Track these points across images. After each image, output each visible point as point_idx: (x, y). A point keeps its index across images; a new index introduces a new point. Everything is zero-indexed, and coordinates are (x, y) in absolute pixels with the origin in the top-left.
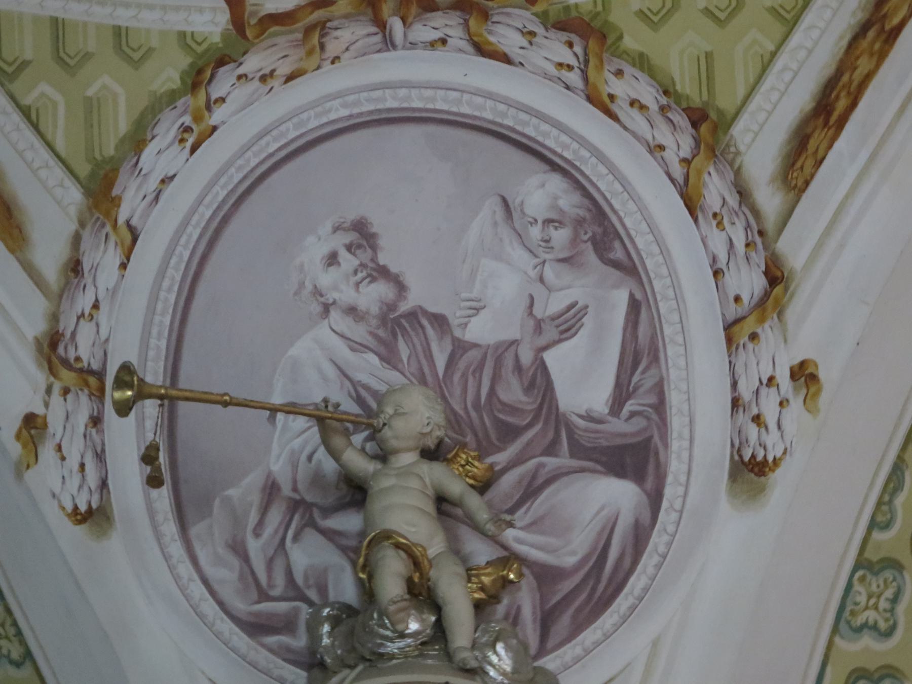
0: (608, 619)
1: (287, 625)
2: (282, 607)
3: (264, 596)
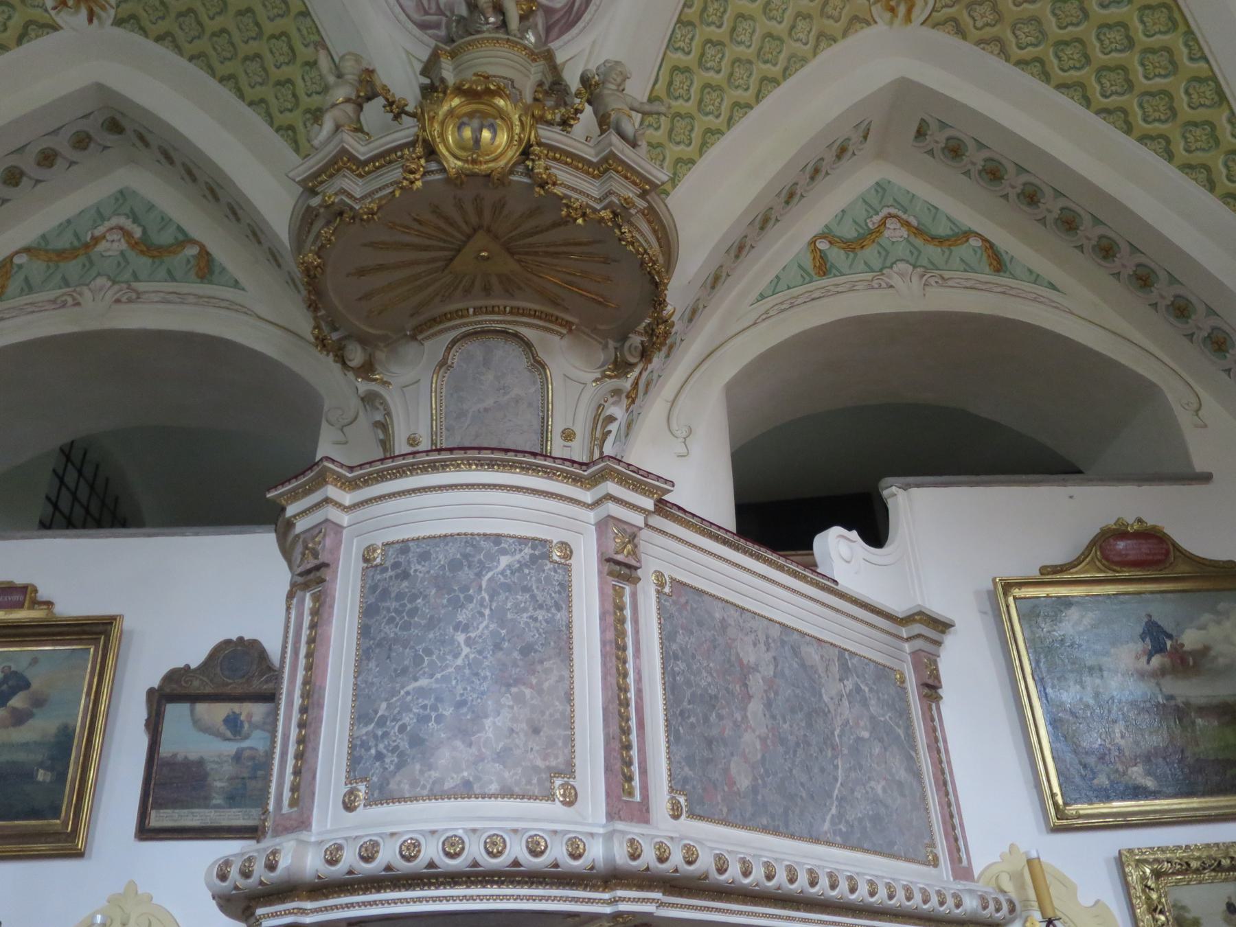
0: (575, 31)
1: (437, 26)
2: (435, 18)
3: (426, 13)
